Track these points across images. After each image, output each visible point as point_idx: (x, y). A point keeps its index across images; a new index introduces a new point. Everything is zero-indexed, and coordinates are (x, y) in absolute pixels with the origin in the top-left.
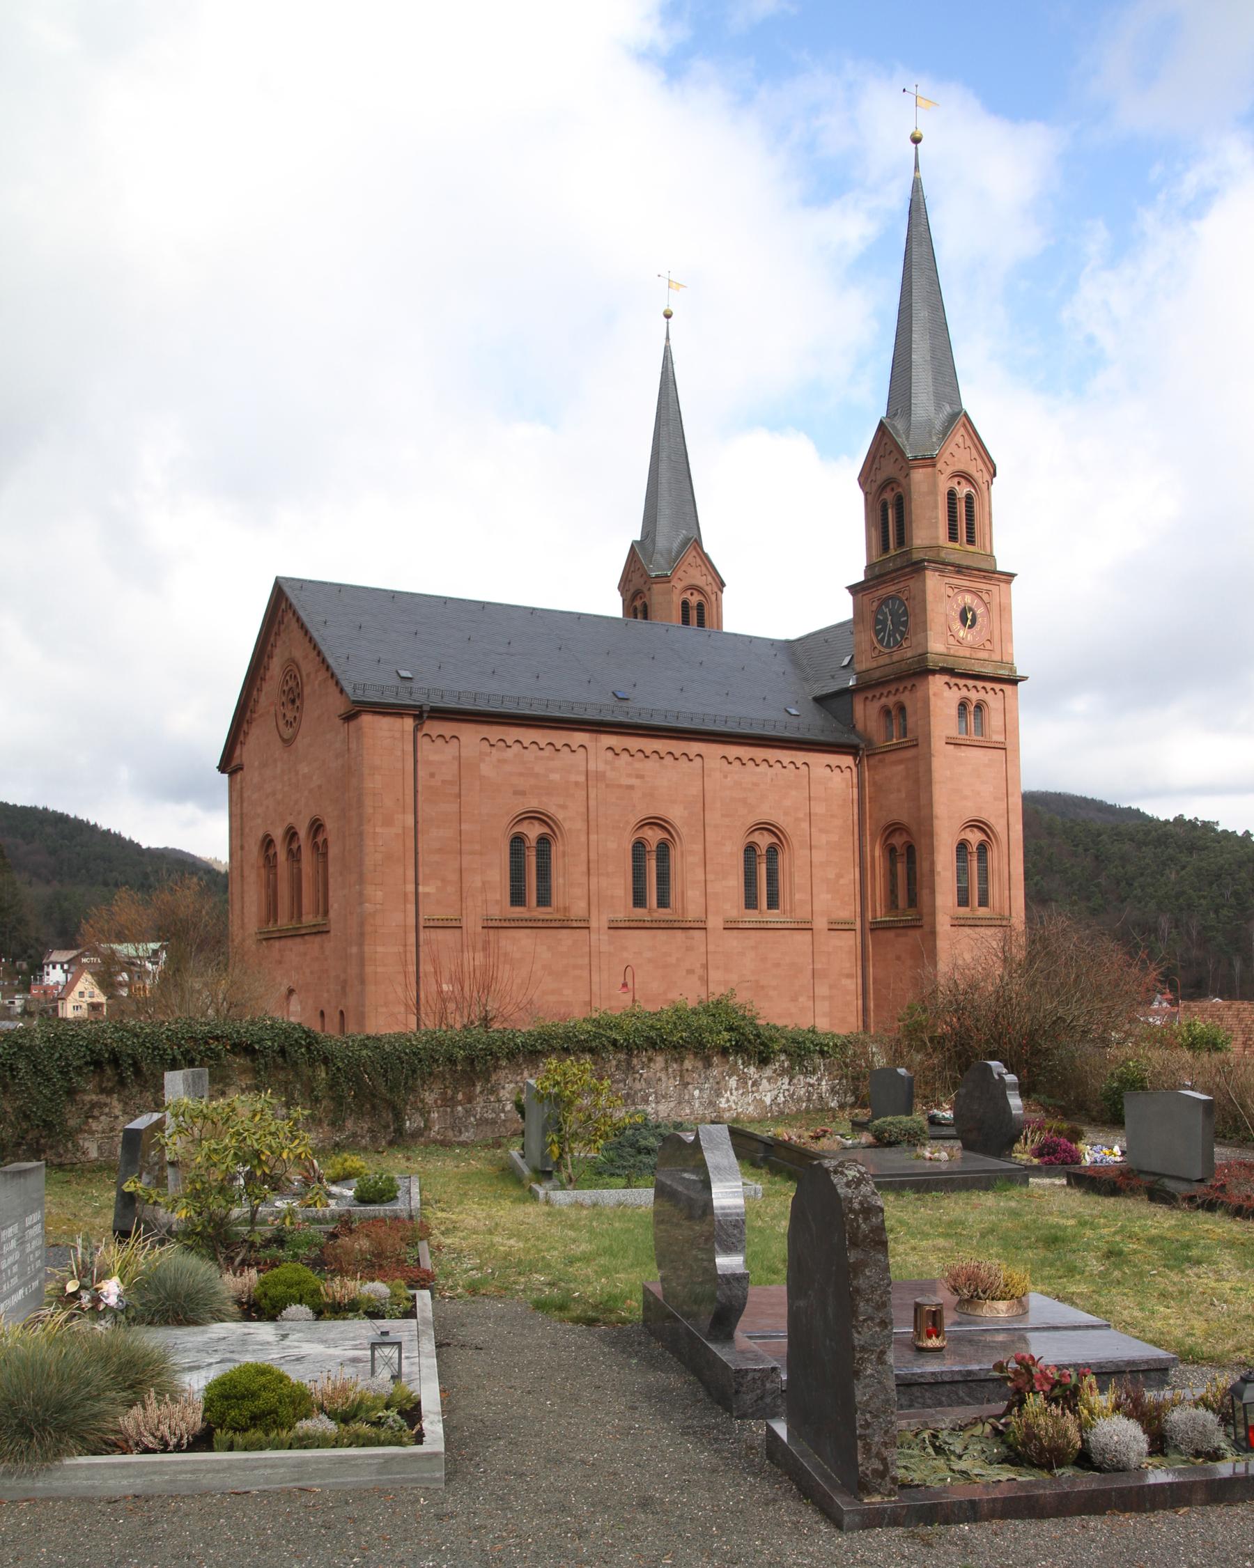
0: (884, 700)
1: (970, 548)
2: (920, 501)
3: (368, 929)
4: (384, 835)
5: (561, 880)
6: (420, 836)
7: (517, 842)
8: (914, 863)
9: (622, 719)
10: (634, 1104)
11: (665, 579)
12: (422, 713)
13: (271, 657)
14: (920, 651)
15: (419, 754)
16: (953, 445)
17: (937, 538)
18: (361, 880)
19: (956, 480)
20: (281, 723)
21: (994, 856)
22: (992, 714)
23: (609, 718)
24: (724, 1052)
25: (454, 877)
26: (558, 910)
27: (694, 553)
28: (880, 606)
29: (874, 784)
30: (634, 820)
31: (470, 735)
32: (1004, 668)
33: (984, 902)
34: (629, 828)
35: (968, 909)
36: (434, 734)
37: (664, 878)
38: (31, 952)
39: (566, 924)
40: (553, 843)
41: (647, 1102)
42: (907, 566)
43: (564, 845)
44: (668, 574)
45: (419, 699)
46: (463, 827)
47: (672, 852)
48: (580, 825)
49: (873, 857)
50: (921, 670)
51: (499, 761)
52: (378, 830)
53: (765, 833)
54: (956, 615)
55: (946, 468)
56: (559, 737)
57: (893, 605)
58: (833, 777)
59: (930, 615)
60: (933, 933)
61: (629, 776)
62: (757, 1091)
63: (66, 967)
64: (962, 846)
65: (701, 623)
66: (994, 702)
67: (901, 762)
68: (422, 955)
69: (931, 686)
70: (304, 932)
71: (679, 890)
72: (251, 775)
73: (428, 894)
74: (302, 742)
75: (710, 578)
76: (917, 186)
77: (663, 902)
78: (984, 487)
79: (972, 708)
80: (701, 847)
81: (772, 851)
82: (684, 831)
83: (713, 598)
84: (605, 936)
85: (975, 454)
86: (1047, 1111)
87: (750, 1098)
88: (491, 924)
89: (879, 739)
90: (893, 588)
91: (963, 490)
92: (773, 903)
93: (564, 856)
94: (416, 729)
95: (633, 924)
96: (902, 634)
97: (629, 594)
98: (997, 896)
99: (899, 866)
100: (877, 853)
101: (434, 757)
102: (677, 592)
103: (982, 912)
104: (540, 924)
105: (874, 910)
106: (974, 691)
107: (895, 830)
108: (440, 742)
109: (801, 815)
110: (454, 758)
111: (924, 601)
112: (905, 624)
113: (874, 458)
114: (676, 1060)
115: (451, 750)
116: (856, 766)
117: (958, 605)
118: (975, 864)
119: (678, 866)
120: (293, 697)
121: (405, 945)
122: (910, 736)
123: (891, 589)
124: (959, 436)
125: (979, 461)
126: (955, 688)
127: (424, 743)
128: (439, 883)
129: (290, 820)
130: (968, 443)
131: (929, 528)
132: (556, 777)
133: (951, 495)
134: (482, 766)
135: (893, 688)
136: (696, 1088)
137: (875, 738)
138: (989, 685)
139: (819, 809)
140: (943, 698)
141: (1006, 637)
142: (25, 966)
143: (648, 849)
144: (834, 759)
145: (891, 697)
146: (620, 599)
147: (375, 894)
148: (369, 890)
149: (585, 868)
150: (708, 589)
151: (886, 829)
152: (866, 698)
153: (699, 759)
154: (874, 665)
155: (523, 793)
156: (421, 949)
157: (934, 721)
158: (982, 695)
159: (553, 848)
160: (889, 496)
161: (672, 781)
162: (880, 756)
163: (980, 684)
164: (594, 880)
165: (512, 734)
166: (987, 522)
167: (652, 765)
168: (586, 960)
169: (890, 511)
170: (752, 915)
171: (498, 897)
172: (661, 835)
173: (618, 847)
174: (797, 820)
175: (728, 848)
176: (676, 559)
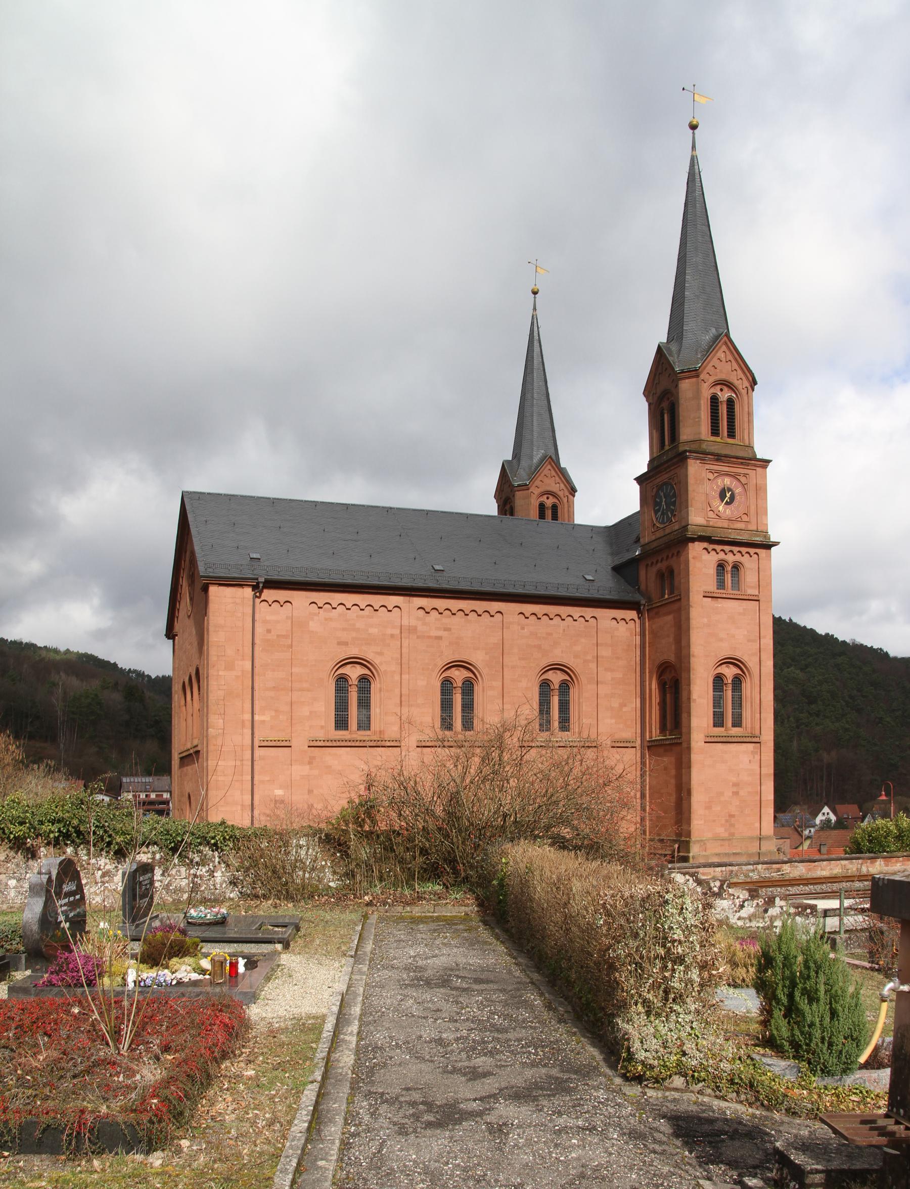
0: (659, 565)
1: (730, 441)
2: (696, 403)
4: (224, 678)
5: (378, 710)
6: (256, 677)
7: (342, 682)
9: (432, 584)
11: (525, 487)
12: (258, 583)
14: (683, 524)
16: (715, 359)
17: (700, 433)
19: (719, 387)
22: (747, 573)
23: (542, 592)
26: (375, 732)
27: (549, 467)
28: (657, 491)
29: (652, 632)
30: (441, 663)
31: (300, 599)
33: (737, 723)
35: (722, 729)
39: (379, 744)
40: (571, 686)
42: (675, 457)
44: (532, 483)
47: (476, 688)
48: (394, 667)
49: (650, 690)
51: (326, 619)
53: (558, 672)
55: (708, 377)
58: (619, 629)
59: (691, 494)
61: (438, 629)
64: (719, 680)
65: (555, 517)
67: (669, 613)
68: (256, 767)
69: (690, 551)
73: (263, 722)
75: (562, 485)
76: (534, 318)
78: (744, 392)
79: (729, 568)
80: (501, 683)
81: (565, 687)
82: (485, 671)
83: (565, 500)
85: (735, 366)
90: (667, 476)
91: (724, 395)
92: (565, 724)
93: (380, 691)
96: (672, 511)
99: (668, 696)
102: (534, 497)
103: (736, 731)
104: (357, 744)
105: (651, 732)
107: (667, 667)
108: (275, 605)
109: (589, 657)
110: (287, 618)
112: (674, 503)
113: (655, 375)
116: (639, 618)
117: (718, 486)
119: (576, 699)
122: (676, 592)
123: (664, 477)
124: (721, 353)
125: (739, 372)
126: (713, 553)
128: (273, 713)
130: (730, 357)
131: (695, 425)
132: (374, 631)
133: (714, 400)
134: (311, 623)
139: (605, 652)
140: (701, 563)
141: (762, 511)
144: (619, 613)
150: (561, 494)
152: (647, 565)
154: (653, 538)
155: (346, 644)
156: (255, 763)
157: (692, 579)
158: (738, 557)
159: (372, 686)
160: (665, 404)
161: (470, 631)
163: (736, 549)
167: (459, 618)
169: (666, 416)
171: (323, 723)
172: (466, 674)
174: (585, 661)
175: (524, 684)
176: (534, 472)
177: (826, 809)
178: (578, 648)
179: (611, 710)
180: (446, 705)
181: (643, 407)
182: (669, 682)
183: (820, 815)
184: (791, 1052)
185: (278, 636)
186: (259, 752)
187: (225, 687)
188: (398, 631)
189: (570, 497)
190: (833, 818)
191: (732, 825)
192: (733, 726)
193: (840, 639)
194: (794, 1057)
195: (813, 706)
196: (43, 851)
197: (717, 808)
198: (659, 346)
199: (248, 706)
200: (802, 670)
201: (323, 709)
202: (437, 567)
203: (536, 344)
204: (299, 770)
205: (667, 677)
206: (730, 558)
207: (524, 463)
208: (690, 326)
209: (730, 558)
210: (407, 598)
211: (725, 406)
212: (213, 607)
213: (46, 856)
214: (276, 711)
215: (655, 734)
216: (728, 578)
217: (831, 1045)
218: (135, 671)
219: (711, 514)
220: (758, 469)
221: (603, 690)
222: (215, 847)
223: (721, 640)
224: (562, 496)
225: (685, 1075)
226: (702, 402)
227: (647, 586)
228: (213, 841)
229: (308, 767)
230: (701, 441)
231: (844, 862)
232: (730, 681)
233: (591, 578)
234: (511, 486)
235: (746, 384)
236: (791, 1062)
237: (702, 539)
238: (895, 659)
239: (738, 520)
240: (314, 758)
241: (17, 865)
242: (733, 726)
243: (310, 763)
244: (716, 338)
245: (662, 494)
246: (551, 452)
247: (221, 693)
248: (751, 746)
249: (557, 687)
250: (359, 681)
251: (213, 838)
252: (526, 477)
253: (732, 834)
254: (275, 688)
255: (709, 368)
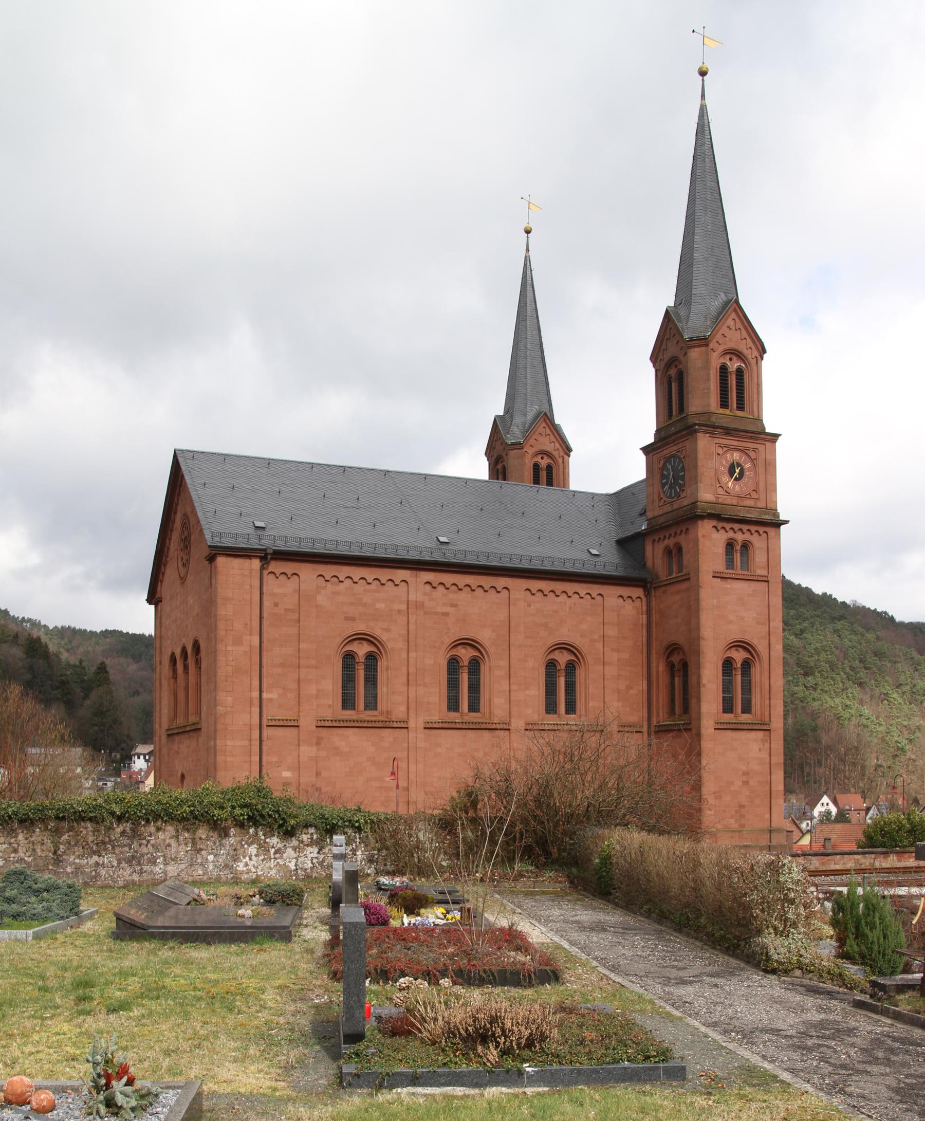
0: (667, 541)
1: (739, 413)
2: (706, 375)
3: (220, 726)
4: (232, 654)
5: (385, 689)
6: (265, 654)
7: (349, 659)
8: (687, 676)
9: (438, 557)
10: (139, 864)
11: (518, 446)
12: (266, 554)
13: (175, 513)
14: (692, 501)
15: (265, 588)
16: (725, 326)
17: (709, 406)
18: (215, 689)
19: (728, 357)
20: (180, 564)
21: (756, 673)
24: (241, 825)
25: (294, 686)
26: (382, 714)
27: (544, 424)
28: (665, 464)
30: (448, 641)
31: (308, 573)
32: (768, 514)
33: (747, 709)
34: (444, 647)
36: (278, 572)
37: (475, 688)
38: (123, 745)
39: (387, 724)
40: (577, 667)
41: (154, 863)
42: (683, 430)
43: (387, 661)
45: (267, 543)
46: (301, 646)
47: (482, 667)
48: (401, 645)
49: (658, 672)
50: (692, 516)
51: (333, 593)
52: (229, 648)
53: (565, 652)
54: (724, 469)
56: (384, 574)
57: (675, 462)
58: (622, 607)
59: (701, 469)
60: (699, 735)
61: (444, 605)
62: (281, 858)
63: (147, 757)
64: (728, 664)
66: (758, 542)
68: (265, 748)
69: (700, 529)
70: (188, 729)
71: (487, 697)
72: (166, 605)
73: (271, 700)
74: (190, 578)
75: (557, 445)
76: (527, 260)
77: (474, 707)
78: (753, 362)
79: (738, 548)
80: (507, 663)
81: (571, 668)
82: (492, 650)
84: (422, 734)
85: (745, 334)
86: (571, 882)
87: (272, 863)
88: (323, 724)
89: (663, 576)
90: (675, 448)
91: (734, 365)
92: (571, 708)
93: (387, 669)
94: (262, 568)
95: (445, 726)
96: (681, 486)
97: (493, 459)
98: (758, 703)
99: (677, 679)
100: (661, 668)
101: (276, 591)
102: (528, 456)
103: (745, 718)
105: (658, 716)
106: (740, 533)
107: (672, 651)
108: (283, 578)
109: (596, 637)
110: (294, 591)
111: (696, 458)
112: (683, 478)
114: (188, 830)
115: (293, 584)
116: (646, 596)
117: (727, 461)
118: (739, 678)
119: (583, 678)
120: (186, 544)
121: (251, 740)
123: (671, 450)
125: (749, 341)
126: (722, 531)
127: (269, 580)
128: (281, 691)
129: (184, 641)
130: (739, 325)
131: (704, 398)
132: (381, 606)
133: (723, 369)
135: (672, 532)
136: (210, 854)
137: (660, 573)
138: (753, 528)
139: (612, 632)
140: (710, 542)
141: (771, 487)
142: (118, 756)
143: (461, 664)
144: (625, 591)
145: (672, 539)
146: (487, 463)
147: (225, 699)
148: (221, 696)
149: (406, 681)
150: (556, 454)
151: (667, 648)
152: (654, 540)
153: (505, 591)
154: (661, 512)
155: (353, 619)
156: (264, 743)
158: (747, 536)
159: (379, 663)
160: (673, 372)
161: (477, 610)
162: (663, 588)
163: (745, 527)
164: (412, 689)
165: (344, 571)
166: (755, 391)
167: (465, 595)
168: (405, 754)
170: (552, 719)
173: (435, 663)
175: (531, 663)
177: (825, 799)
178: (584, 627)
179: (614, 691)
180: (453, 684)
181: (649, 373)
182: (674, 665)
183: (819, 805)
184: (860, 961)
185: (285, 610)
186: (267, 732)
187: (233, 663)
188: (405, 607)
189: (566, 457)
190: (834, 810)
191: (743, 816)
192: (742, 712)
193: (840, 600)
194: (862, 964)
195: (810, 678)
196: (232, 831)
197: (727, 798)
198: (667, 310)
199: (256, 683)
200: (796, 635)
201: (331, 687)
202: (442, 539)
203: (529, 288)
204: (308, 751)
205: (676, 659)
206: (740, 537)
207: (518, 420)
208: (699, 289)
209: (740, 537)
210: (414, 572)
211: (734, 377)
212: (221, 578)
213: (234, 835)
214: (284, 689)
215: (661, 717)
216: (737, 557)
217: (884, 955)
218: (30, 620)
219: (720, 491)
220: (767, 443)
221: (611, 671)
222: (359, 829)
223: (730, 622)
224: (557, 456)
225: (802, 969)
226: (712, 372)
227: (653, 563)
228: (357, 824)
229: (315, 748)
230: (710, 414)
231: (857, 857)
232: (739, 666)
233: (597, 553)
234: (503, 442)
235: (756, 353)
236: (860, 967)
237: (711, 516)
238: (902, 624)
239: (748, 497)
240: (322, 738)
241: (215, 843)
242: (742, 712)
243: (318, 744)
244: (726, 304)
245: (670, 467)
246: (545, 408)
247: (230, 669)
248: (760, 734)
249: (563, 667)
250: (366, 659)
251: (357, 821)
252: (520, 435)
253: (743, 826)
254: (282, 665)
255: (719, 337)
